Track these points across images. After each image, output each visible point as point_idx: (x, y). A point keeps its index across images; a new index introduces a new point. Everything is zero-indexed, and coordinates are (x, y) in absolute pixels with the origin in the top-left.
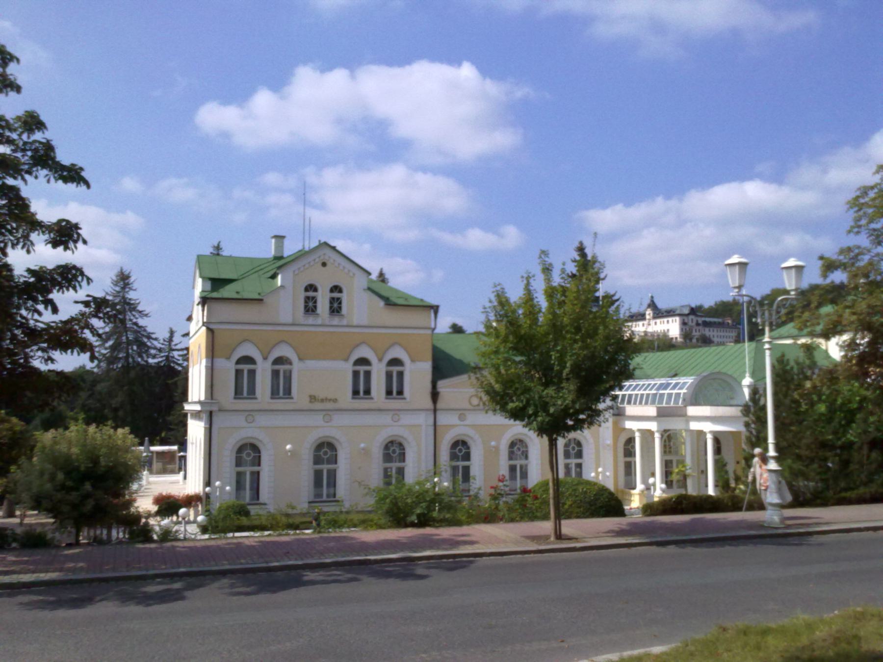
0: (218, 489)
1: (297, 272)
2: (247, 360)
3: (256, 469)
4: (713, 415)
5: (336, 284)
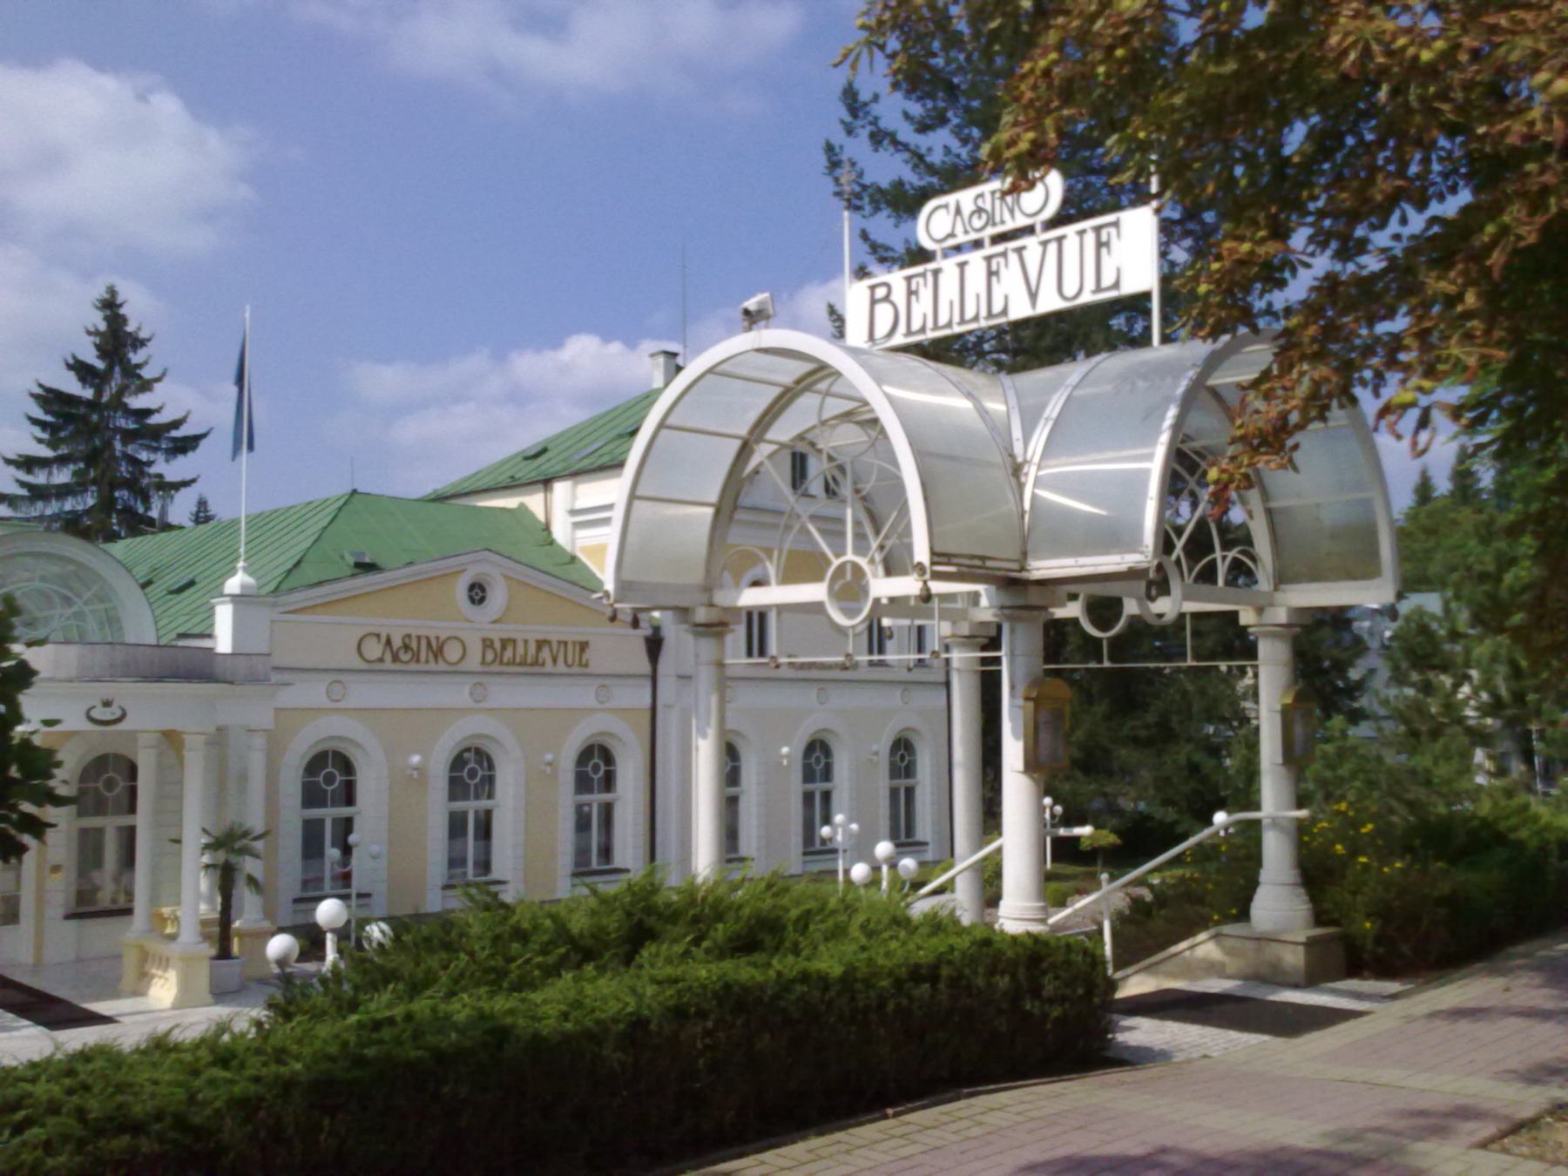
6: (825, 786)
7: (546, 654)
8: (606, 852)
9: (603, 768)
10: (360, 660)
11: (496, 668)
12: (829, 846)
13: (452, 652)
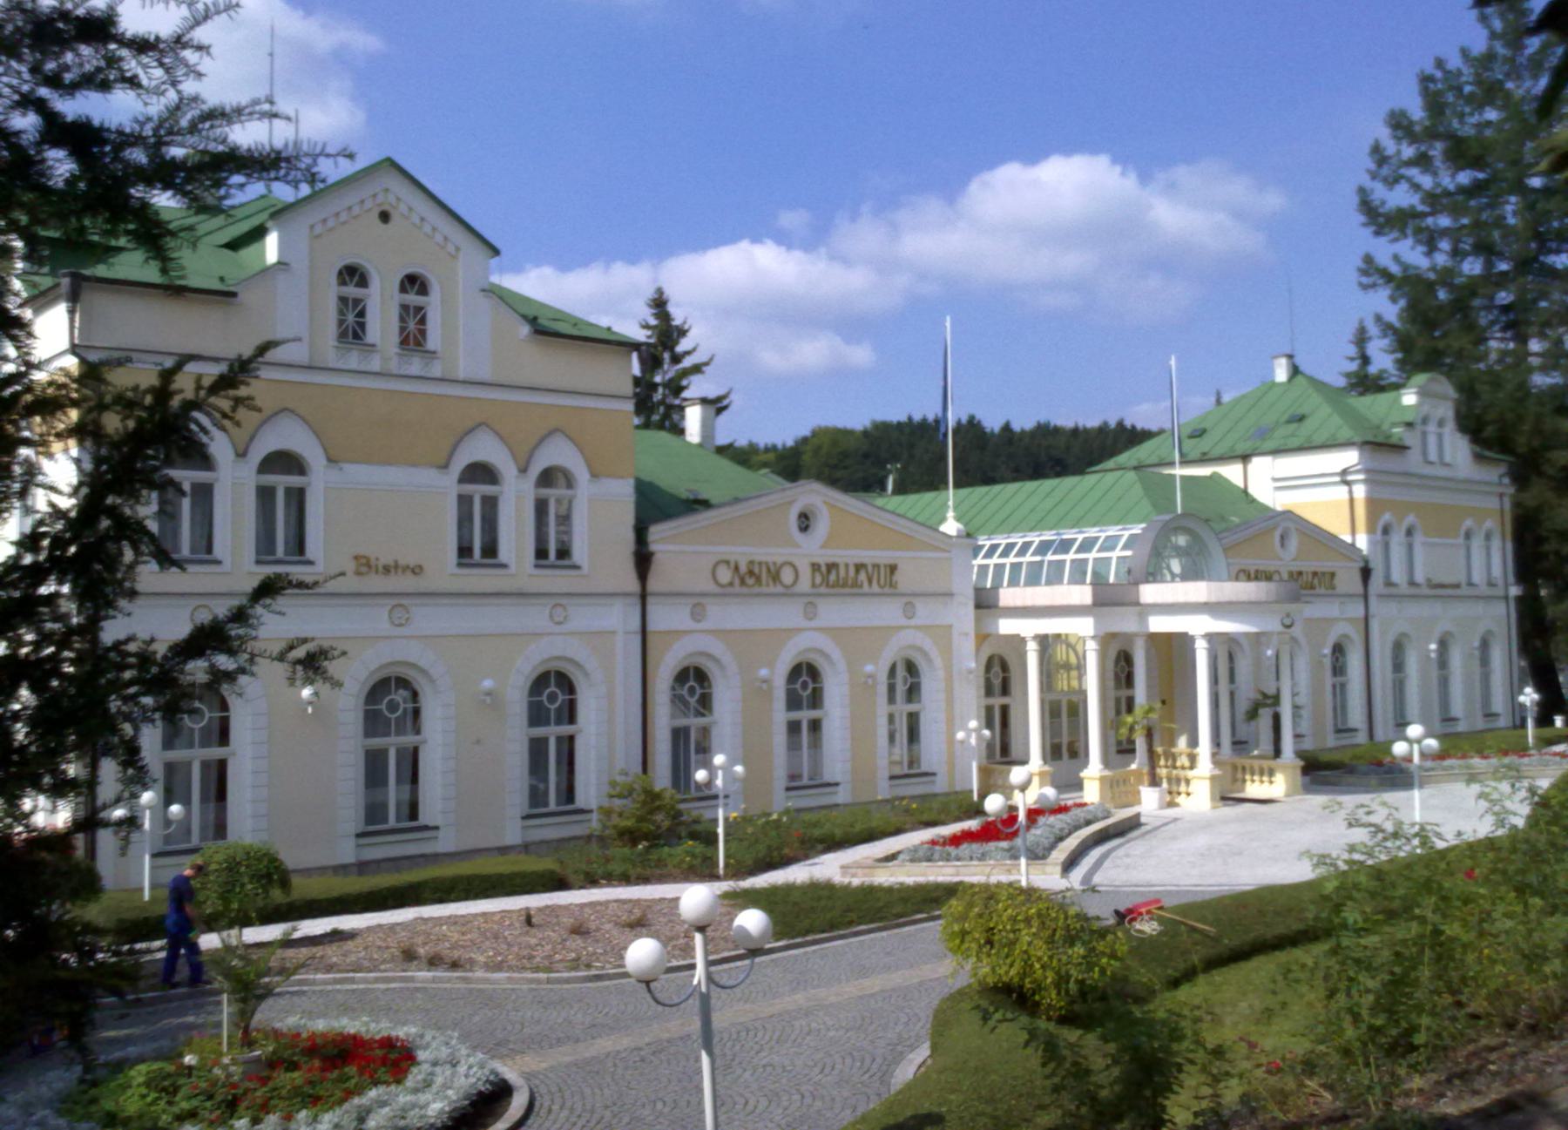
0: (148, 813)
1: (318, 229)
2: (481, 472)
3: (216, 752)
4: (1213, 599)
5: (349, 261)
6: (814, 714)
7: (863, 576)
8: (568, 793)
9: (991, 675)
10: (712, 582)
11: (823, 590)
12: (707, 792)
13: (787, 576)
